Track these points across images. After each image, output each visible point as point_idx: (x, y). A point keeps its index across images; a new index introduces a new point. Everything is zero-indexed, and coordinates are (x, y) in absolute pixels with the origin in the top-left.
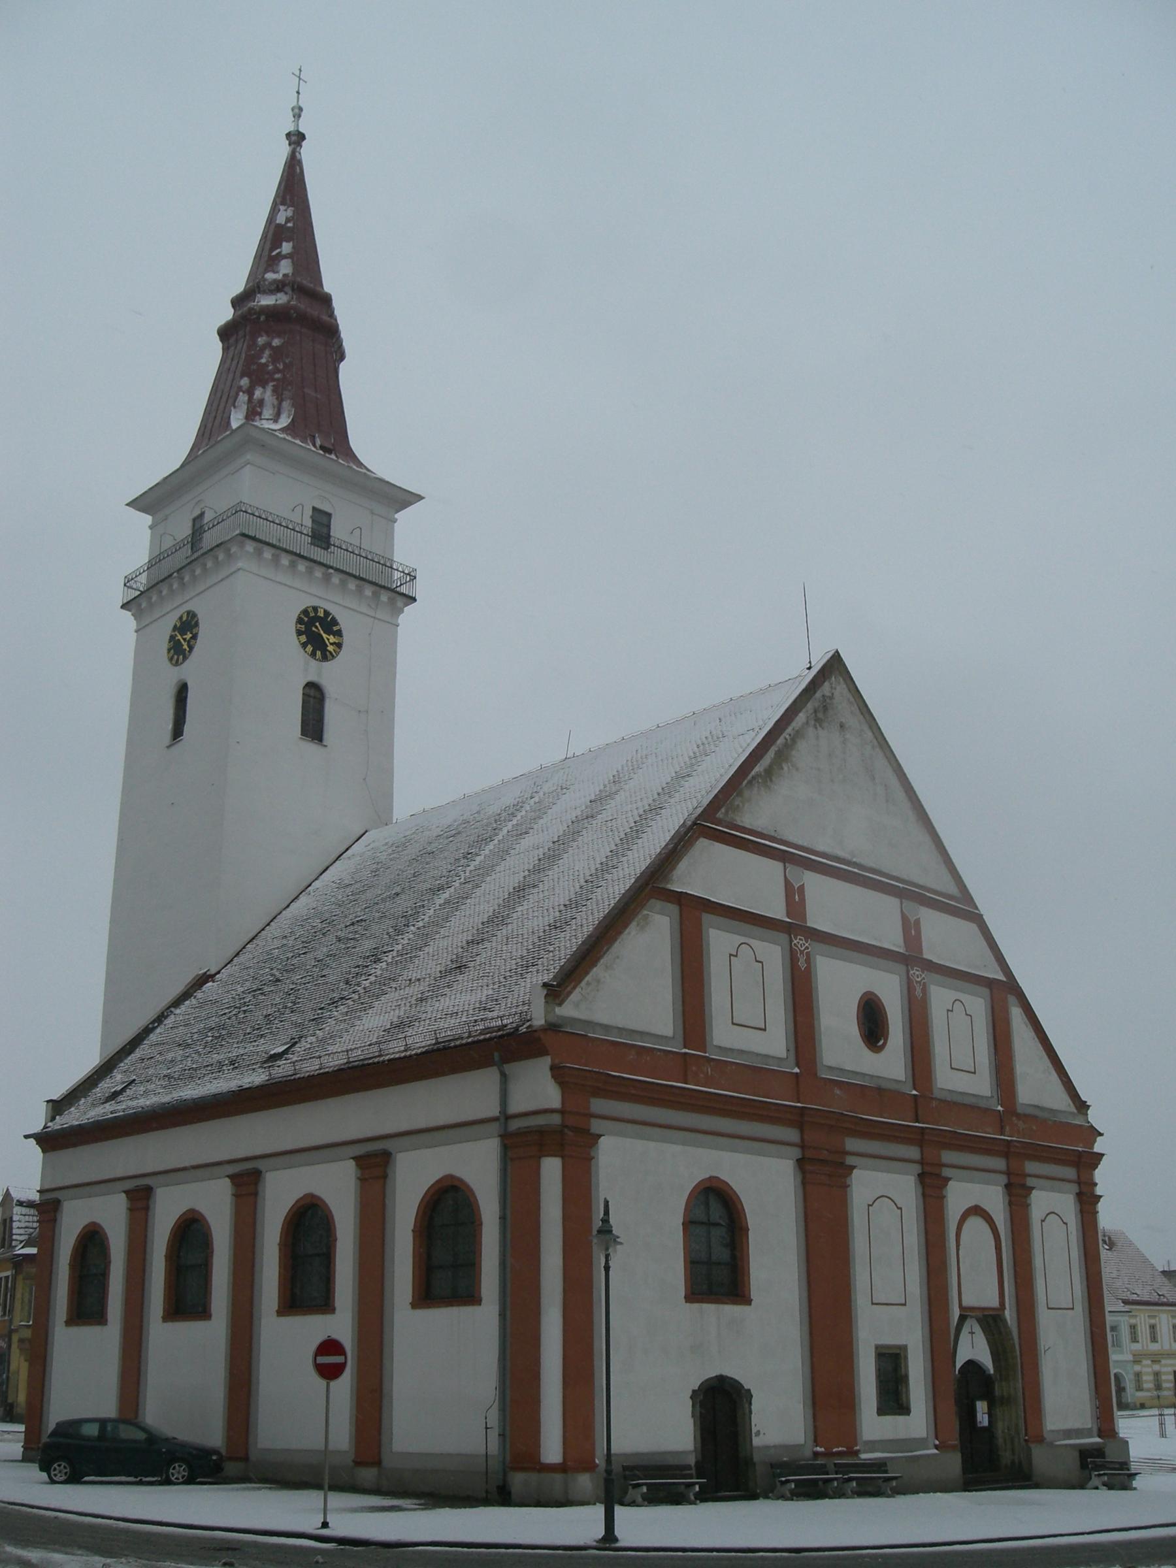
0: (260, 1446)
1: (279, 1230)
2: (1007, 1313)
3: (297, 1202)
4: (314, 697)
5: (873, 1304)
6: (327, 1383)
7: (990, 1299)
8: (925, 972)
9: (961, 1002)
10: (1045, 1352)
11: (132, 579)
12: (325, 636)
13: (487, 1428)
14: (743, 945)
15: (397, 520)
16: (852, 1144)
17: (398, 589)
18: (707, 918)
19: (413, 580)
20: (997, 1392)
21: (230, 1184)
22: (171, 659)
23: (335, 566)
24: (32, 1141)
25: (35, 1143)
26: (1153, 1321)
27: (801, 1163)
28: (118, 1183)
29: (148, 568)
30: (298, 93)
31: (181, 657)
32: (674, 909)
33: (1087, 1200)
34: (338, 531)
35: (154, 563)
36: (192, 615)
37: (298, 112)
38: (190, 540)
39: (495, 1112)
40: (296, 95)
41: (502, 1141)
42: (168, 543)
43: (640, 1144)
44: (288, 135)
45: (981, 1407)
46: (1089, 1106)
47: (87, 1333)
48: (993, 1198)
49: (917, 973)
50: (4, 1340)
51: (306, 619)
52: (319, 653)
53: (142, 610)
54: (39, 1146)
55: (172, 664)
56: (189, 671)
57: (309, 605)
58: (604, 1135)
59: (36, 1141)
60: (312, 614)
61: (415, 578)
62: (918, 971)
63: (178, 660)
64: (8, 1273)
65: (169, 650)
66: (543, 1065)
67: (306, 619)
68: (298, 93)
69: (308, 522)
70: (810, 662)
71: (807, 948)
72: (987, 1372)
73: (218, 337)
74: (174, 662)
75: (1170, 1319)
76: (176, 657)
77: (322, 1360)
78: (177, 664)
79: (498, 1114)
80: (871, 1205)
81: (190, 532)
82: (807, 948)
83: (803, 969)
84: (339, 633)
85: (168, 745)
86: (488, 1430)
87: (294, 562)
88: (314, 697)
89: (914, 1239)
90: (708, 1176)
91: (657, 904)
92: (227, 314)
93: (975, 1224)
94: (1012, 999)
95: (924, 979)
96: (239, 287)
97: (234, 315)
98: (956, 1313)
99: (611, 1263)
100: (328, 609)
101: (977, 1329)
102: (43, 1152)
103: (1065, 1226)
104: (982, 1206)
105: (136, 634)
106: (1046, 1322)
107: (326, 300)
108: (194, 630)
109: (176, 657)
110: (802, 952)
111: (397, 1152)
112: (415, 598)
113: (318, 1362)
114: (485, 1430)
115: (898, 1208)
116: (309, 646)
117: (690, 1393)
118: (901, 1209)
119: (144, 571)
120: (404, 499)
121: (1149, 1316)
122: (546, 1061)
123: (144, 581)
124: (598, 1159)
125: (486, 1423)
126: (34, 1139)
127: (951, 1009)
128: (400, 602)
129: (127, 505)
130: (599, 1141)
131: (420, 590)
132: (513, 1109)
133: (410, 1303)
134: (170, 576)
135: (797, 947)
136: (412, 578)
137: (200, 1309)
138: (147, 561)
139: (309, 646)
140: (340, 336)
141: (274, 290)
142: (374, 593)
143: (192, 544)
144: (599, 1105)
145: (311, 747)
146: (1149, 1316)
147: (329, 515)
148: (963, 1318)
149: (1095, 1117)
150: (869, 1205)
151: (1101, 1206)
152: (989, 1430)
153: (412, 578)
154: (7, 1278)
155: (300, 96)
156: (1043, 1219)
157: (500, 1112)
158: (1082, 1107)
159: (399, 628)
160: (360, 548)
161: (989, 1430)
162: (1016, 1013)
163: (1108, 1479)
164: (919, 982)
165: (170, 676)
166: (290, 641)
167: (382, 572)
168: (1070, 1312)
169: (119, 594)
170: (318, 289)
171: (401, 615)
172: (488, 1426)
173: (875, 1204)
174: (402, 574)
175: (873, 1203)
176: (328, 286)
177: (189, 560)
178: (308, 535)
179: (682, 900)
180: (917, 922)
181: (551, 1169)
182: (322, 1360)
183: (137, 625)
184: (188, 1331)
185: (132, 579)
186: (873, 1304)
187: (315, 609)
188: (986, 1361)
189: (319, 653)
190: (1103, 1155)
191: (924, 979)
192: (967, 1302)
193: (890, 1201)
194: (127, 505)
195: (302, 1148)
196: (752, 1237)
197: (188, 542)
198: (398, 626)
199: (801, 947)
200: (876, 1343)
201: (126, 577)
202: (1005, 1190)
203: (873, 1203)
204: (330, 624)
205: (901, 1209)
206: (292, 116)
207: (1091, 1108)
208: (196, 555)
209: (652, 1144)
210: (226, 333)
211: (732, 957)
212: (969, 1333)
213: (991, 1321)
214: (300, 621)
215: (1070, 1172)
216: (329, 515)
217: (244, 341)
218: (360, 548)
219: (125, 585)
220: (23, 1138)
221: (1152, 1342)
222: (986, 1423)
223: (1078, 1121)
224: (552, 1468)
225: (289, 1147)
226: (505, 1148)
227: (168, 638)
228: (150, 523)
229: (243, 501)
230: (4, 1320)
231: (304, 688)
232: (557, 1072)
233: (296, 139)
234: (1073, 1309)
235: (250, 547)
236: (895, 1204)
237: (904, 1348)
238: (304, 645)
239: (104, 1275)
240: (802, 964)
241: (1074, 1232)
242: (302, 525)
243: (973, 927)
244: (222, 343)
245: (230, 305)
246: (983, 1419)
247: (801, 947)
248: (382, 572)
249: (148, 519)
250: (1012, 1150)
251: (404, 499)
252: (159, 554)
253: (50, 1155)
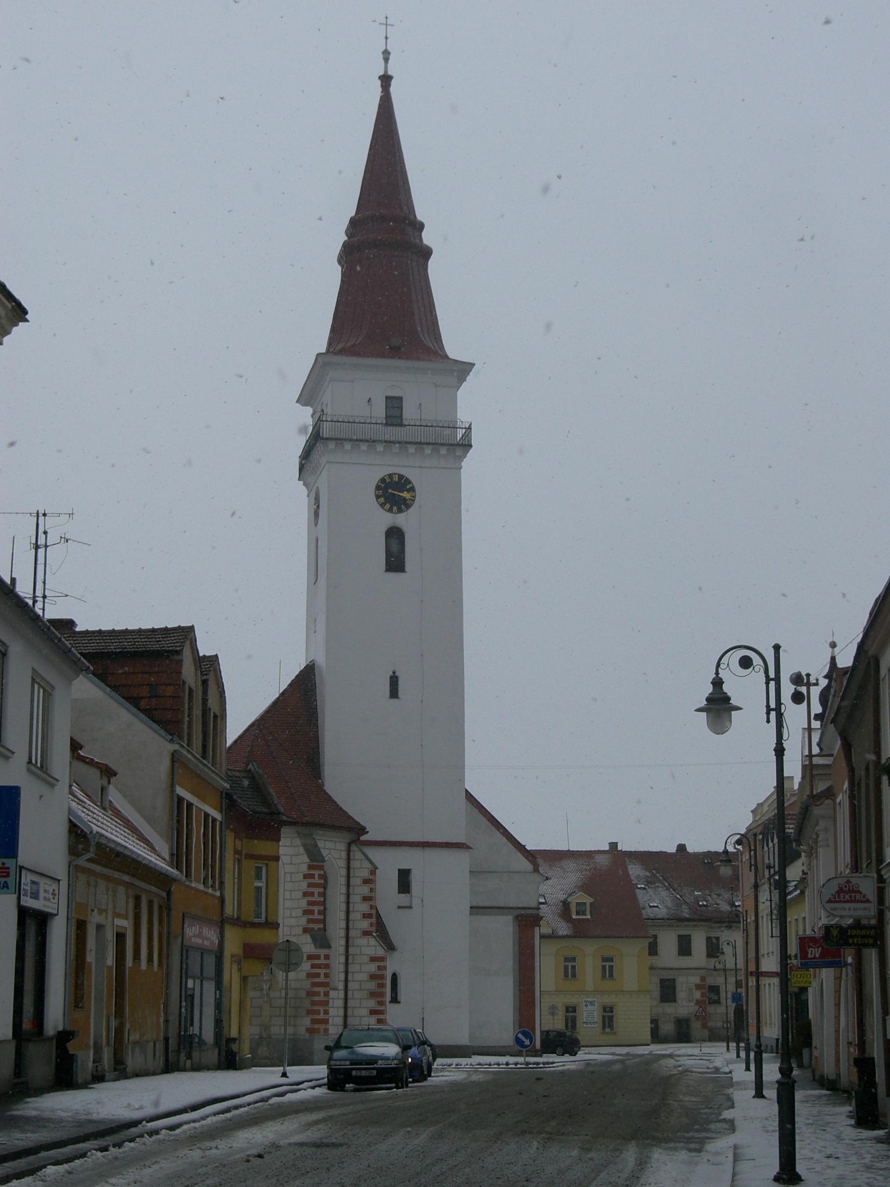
4: (395, 535)
12: (401, 494)
14: (59, 541)
30: (386, 38)
34: (409, 413)
37: (386, 55)
40: (388, 36)
51: (383, 485)
52: (395, 508)
57: (385, 474)
84: (412, 489)
88: (395, 535)
133: (186, 634)
141: (161, 1130)
142: (448, 450)
147: (400, 399)
172: (290, 862)
176: (420, 216)
183: (308, 490)
187: (390, 476)
204: (403, 483)
214: (378, 488)
216: (400, 399)
233: (386, 80)
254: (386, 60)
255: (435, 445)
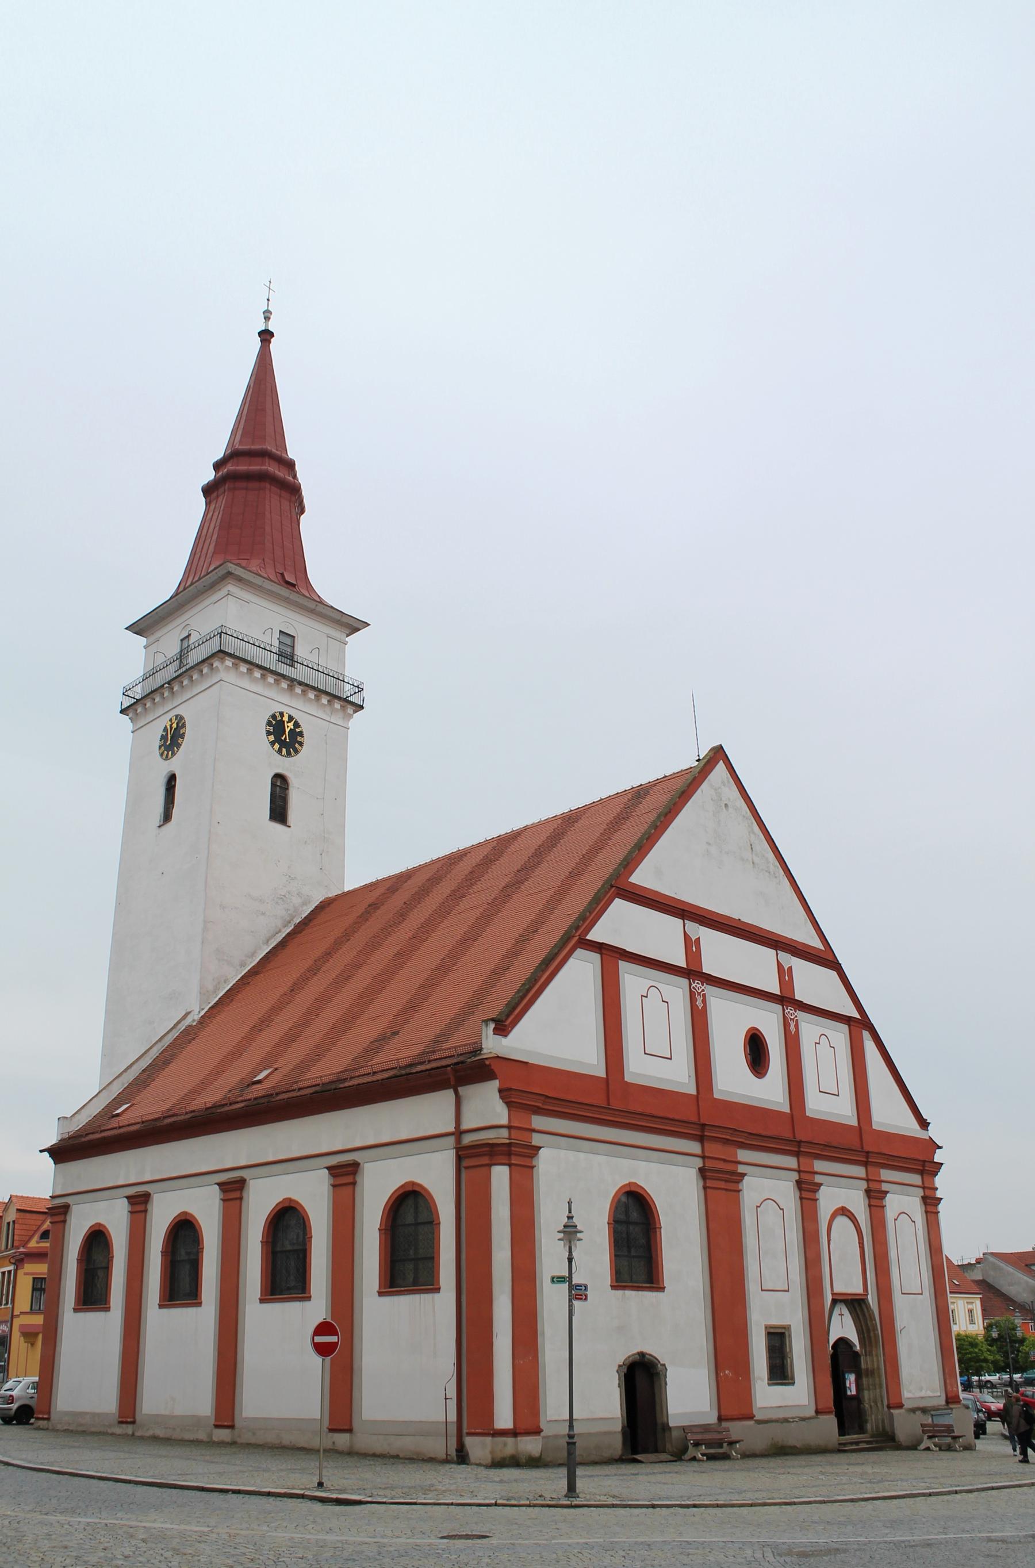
0: (244, 1415)
1: (114, 1242)
2: (870, 1297)
3: (277, 1205)
4: (280, 785)
5: (762, 1290)
6: (323, 1359)
7: (855, 1288)
8: (797, 1011)
9: (826, 1036)
10: (901, 1331)
11: (130, 689)
13: (446, 1399)
15: (347, 642)
16: (743, 1155)
17: (349, 699)
18: (623, 966)
19: (361, 691)
20: (863, 1366)
21: (219, 1190)
22: (162, 755)
23: (298, 679)
24: (46, 1154)
25: (48, 1155)
26: (970, 1307)
27: (702, 1171)
28: (121, 1190)
29: (143, 680)
30: (268, 300)
31: (170, 752)
32: (596, 957)
33: (931, 1202)
34: (301, 651)
35: (148, 676)
36: (180, 718)
37: (267, 316)
38: (179, 657)
39: (451, 1128)
40: (267, 301)
41: (457, 1153)
42: (160, 660)
43: (571, 1155)
44: (260, 334)
45: (851, 1379)
46: (929, 1123)
47: (92, 1318)
48: (856, 1200)
49: (791, 1012)
50: (6, 1325)
51: (274, 722)
52: (284, 750)
53: (164, 698)
54: (52, 1158)
55: (162, 758)
56: (176, 764)
58: (543, 1147)
59: (49, 1154)
60: (279, 718)
61: (363, 689)
62: (792, 1010)
63: (168, 754)
64: (11, 1268)
65: (160, 747)
66: (492, 1087)
67: (274, 722)
68: (268, 300)
69: (276, 643)
70: (699, 756)
71: (703, 990)
72: (854, 1349)
73: (202, 493)
74: (164, 757)
75: (966, 1305)
76: (166, 752)
77: (319, 1339)
78: (167, 758)
79: (454, 1130)
80: (759, 1207)
81: (179, 650)
82: (703, 990)
83: (700, 1008)
84: (291, 718)
85: (158, 825)
86: (447, 1400)
87: (264, 675)
88: (280, 785)
89: (794, 1236)
90: (627, 1182)
91: (580, 952)
92: (210, 475)
93: (842, 1221)
94: (866, 1034)
95: (796, 1017)
96: (220, 455)
97: (215, 476)
98: (828, 1299)
99: (574, 1254)
100: (292, 714)
101: (845, 1311)
102: (55, 1163)
103: (913, 1223)
104: (847, 1207)
105: (132, 734)
106: (900, 1303)
107: (290, 465)
108: (181, 730)
109: (166, 752)
110: (699, 994)
111: (365, 1163)
112: (362, 706)
113: (315, 1341)
114: (444, 1400)
115: (780, 1209)
116: (277, 744)
117: (616, 1368)
118: (783, 1209)
119: (140, 683)
120: (353, 626)
121: (967, 1302)
122: (495, 1084)
123: (139, 691)
124: (538, 1167)
125: (446, 1394)
126: (48, 1152)
127: (818, 1042)
128: (350, 710)
129: (126, 629)
130: (539, 1152)
131: (369, 697)
132: (465, 1126)
134: (163, 685)
135: (696, 990)
136: (360, 690)
137: (555, 1280)
138: (142, 674)
139: (277, 744)
140: (301, 493)
143: (181, 660)
144: (539, 1122)
145: (278, 827)
146: (967, 1302)
148: (834, 1302)
149: (934, 1133)
150: (757, 1207)
151: (941, 1207)
152: (858, 1399)
153: (360, 690)
154: (9, 1272)
155: (270, 303)
156: (896, 1218)
157: (455, 1128)
158: (924, 1124)
159: (349, 730)
160: (318, 665)
161: (858, 1399)
162: (870, 1046)
163: (938, 1440)
164: (793, 1019)
165: (162, 769)
166: (262, 741)
167: (336, 685)
168: (920, 1296)
169: (119, 700)
170: (284, 455)
171: (351, 720)
172: (447, 1397)
173: (762, 1206)
174: (352, 686)
175: (760, 1205)
176: (291, 454)
177: (178, 673)
178: (276, 653)
179: (600, 948)
180: (790, 968)
181: (500, 1176)
182: (319, 1339)
184: (181, 1316)
185: (130, 689)
186: (762, 1290)
188: (854, 1337)
189: (284, 750)
190: (942, 1164)
191: (796, 1017)
192: (838, 1289)
193: (774, 1203)
194: (126, 629)
195: (358, 1147)
196: (664, 1233)
197: (177, 659)
198: (348, 729)
199: (699, 989)
200: (766, 1323)
201: (124, 688)
202: (865, 1194)
203: (760, 1205)
205: (783, 1209)
206: (263, 318)
207: (930, 1125)
208: (184, 669)
209: (582, 1155)
210: (208, 491)
211: (643, 998)
212: (839, 1315)
213: (856, 1304)
215: (916, 1179)
217: (224, 496)
218: (318, 665)
219: (123, 694)
220: (39, 1152)
221: (971, 1324)
222: (854, 1392)
223: (920, 1134)
224: (503, 1433)
225: (271, 1159)
226: (459, 1158)
227: (160, 737)
228: (145, 644)
229: (224, 625)
230: (7, 1308)
231: (272, 779)
232: (504, 1093)
233: (266, 336)
234: (922, 1294)
235: (229, 662)
236: (779, 1206)
237: (788, 1328)
238: (272, 743)
239: (107, 1269)
240: (699, 1003)
241: (921, 1228)
242: (271, 645)
243: (834, 974)
244: (205, 498)
245: (212, 467)
246: (852, 1391)
247: (699, 989)
248: (336, 685)
249: (142, 641)
250: (870, 1160)
251: (353, 626)
252: (153, 669)
253: (62, 1166)
254: (267, 319)
255: (320, 692)
